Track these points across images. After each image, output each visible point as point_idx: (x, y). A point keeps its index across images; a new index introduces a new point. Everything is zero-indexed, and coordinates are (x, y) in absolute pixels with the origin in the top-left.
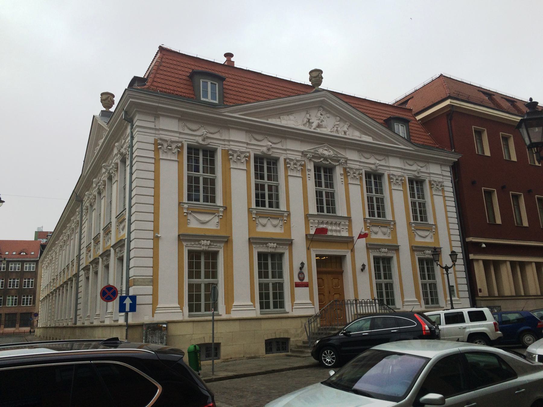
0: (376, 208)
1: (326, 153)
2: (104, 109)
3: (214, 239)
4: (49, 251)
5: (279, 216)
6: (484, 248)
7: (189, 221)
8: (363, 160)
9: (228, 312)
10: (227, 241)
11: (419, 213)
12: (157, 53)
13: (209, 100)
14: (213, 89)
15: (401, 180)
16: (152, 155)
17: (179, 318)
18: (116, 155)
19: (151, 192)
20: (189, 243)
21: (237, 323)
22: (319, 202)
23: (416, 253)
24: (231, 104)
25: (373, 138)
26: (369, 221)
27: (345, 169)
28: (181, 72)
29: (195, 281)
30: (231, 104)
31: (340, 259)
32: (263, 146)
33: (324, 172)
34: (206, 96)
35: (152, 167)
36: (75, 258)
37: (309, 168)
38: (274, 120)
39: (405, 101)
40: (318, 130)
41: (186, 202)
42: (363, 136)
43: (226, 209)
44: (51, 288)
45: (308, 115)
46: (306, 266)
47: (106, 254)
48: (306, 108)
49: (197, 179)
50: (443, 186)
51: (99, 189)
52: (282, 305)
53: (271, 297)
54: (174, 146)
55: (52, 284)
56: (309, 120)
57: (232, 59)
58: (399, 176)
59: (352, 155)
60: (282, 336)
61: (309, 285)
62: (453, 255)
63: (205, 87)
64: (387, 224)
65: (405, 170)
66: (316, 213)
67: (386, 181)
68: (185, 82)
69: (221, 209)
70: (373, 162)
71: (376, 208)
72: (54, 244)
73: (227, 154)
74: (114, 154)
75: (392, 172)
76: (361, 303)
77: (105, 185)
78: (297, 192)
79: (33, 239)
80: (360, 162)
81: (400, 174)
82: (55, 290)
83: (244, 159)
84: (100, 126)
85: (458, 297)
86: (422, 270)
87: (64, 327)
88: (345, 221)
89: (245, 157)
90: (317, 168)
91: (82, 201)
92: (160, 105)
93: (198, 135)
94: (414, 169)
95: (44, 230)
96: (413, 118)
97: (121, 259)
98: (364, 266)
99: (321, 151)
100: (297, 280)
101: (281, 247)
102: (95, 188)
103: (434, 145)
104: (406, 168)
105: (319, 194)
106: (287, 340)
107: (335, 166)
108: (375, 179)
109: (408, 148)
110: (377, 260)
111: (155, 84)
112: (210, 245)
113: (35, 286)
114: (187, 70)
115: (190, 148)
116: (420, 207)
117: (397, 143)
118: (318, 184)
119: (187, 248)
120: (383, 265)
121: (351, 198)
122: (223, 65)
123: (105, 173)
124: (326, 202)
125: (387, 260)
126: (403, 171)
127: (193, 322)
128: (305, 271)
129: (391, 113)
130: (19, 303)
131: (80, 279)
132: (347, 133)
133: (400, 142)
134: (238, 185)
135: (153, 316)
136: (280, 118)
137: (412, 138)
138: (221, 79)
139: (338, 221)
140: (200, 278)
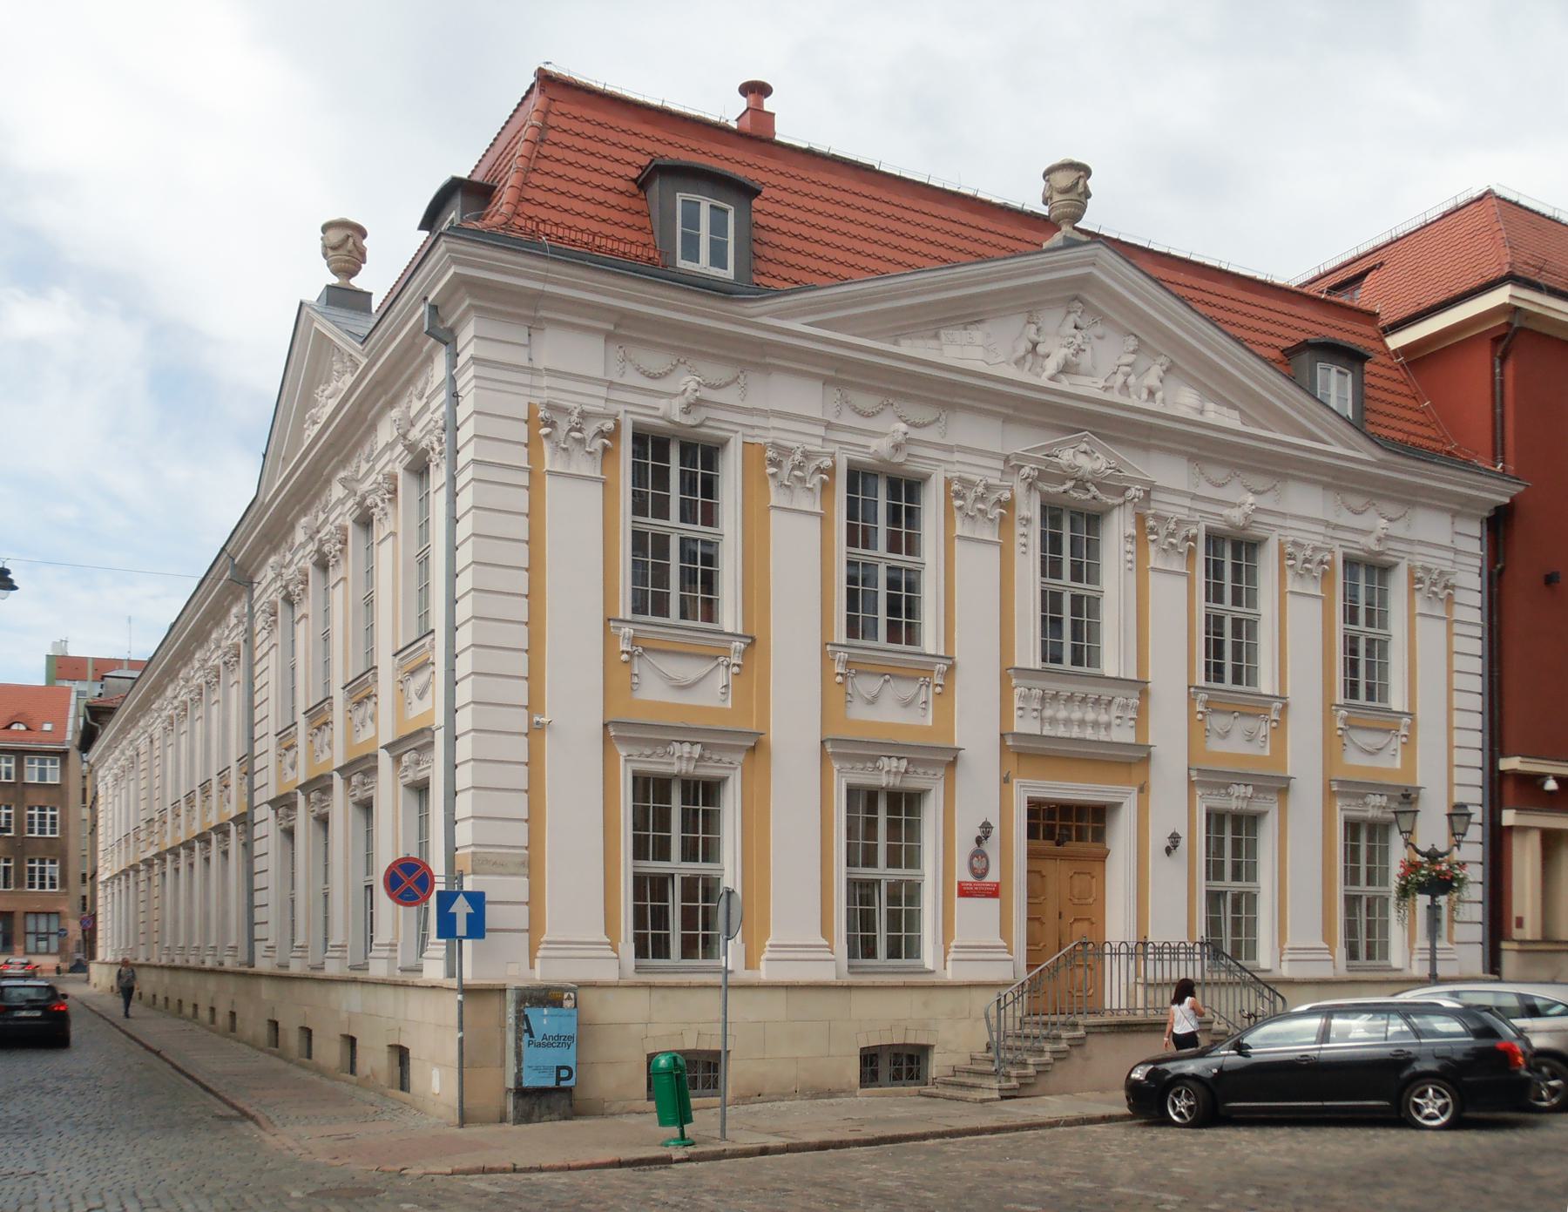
0: (1226, 651)
1: (1086, 464)
2: (334, 280)
3: (712, 738)
4: (123, 731)
5: (918, 672)
6: (1551, 792)
7: (636, 680)
8: (1206, 490)
9: (750, 963)
10: (755, 748)
11: (1361, 668)
12: (529, 92)
13: (703, 265)
14: (718, 227)
15: (1322, 562)
16: (520, 457)
17: (609, 974)
18: (390, 446)
19: (521, 582)
20: (635, 751)
21: (781, 995)
22: (1051, 624)
23: (1339, 803)
24: (788, 286)
25: (1241, 412)
26: (1203, 696)
27: (1140, 520)
28: (609, 166)
29: (653, 866)
30: (788, 286)
31: (1096, 817)
32: (880, 436)
33: (1070, 530)
34: (692, 253)
35: (521, 500)
36: (234, 766)
37: (1025, 513)
38: (919, 343)
39: (1351, 277)
40: (1065, 385)
41: (629, 616)
42: (1210, 406)
43: (752, 642)
44: (143, 846)
45: (1034, 327)
46: (995, 833)
47: (361, 766)
48: (1027, 303)
49: (662, 542)
50: (1453, 587)
51: (319, 551)
52: (913, 950)
53: (879, 922)
54: (591, 428)
55: (142, 836)
56: (1035, 345)
57: (768, 104)
58: (1315, 549)
59: (1168, 473)
60: (912, 1039)
61: (1002, 891)
62: (1458, 814)
63: (692, 221)
64: (1256, 707)
65: (1336, 527)
66: (1038, 665)
67: (1267, 565)
68: (624, 202)
69: (738, 645)
70: (1238, 503)
71: (1226, 651)
72: (144, 707)
73: (763, 461)
74: (380, 445)
75: (1291, 536)
76: (1159, 951)
77: (345, 542)
78: (976, 589)
79: (40, 681)
80: (1194, 497)
81: (1317, 541)
82: (161, 856)
83: (817, 479)
84: (320, 337)
85: (1450, 940)
86: (1352, 853)
87: (212, 971)
88: (1128, 693)
89: (819, 470)
90: (1051, 513)
91: (249, 584)
92: (549, 288)
93: (670, 396)
94: (1372, 527)
95: (73, 652)
96: (1378, 346)
97: (421, 789)
98: (1175, 838)
99: (1066, 457)
100: (962, 874)
101: (920, 770)
102: (303, 545)
103: (1438, 446)
104: (1341, 521)
105: (1051, 601)
106: (925, 1050)
107: (1113, 507)
108: (1236, 554)
109: (1362, 453)
110: (1216, 819)
111: (529, 209)
112: (701, 757)
113: (64, 828)
114: (628, 156)
115: (639, 438)
116: (1369, 653)
117: (1326, 437)
118: (1051, 567)
119: (630, 767)
120: (1232, 834)
121: (1149, 612)
122: (739, 135)
123: (341, 502)
124: (1069, 628)
125: (1246, 823)
126: (1330, 532)
127: (650, 986)
128: (992, 848)
129: (1318, 329)
130: (19, 883)
131: (258, 831)
132: (1159, 395)
133: (1330, 434)
134: (787, 560)
135: (532, 967)
136: (936, 336)
137: (1368, 415)
138: (745, 192)
139: (1106, 692)
140: (668, 859)
